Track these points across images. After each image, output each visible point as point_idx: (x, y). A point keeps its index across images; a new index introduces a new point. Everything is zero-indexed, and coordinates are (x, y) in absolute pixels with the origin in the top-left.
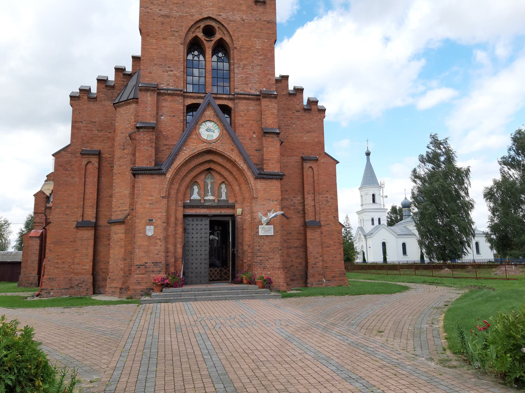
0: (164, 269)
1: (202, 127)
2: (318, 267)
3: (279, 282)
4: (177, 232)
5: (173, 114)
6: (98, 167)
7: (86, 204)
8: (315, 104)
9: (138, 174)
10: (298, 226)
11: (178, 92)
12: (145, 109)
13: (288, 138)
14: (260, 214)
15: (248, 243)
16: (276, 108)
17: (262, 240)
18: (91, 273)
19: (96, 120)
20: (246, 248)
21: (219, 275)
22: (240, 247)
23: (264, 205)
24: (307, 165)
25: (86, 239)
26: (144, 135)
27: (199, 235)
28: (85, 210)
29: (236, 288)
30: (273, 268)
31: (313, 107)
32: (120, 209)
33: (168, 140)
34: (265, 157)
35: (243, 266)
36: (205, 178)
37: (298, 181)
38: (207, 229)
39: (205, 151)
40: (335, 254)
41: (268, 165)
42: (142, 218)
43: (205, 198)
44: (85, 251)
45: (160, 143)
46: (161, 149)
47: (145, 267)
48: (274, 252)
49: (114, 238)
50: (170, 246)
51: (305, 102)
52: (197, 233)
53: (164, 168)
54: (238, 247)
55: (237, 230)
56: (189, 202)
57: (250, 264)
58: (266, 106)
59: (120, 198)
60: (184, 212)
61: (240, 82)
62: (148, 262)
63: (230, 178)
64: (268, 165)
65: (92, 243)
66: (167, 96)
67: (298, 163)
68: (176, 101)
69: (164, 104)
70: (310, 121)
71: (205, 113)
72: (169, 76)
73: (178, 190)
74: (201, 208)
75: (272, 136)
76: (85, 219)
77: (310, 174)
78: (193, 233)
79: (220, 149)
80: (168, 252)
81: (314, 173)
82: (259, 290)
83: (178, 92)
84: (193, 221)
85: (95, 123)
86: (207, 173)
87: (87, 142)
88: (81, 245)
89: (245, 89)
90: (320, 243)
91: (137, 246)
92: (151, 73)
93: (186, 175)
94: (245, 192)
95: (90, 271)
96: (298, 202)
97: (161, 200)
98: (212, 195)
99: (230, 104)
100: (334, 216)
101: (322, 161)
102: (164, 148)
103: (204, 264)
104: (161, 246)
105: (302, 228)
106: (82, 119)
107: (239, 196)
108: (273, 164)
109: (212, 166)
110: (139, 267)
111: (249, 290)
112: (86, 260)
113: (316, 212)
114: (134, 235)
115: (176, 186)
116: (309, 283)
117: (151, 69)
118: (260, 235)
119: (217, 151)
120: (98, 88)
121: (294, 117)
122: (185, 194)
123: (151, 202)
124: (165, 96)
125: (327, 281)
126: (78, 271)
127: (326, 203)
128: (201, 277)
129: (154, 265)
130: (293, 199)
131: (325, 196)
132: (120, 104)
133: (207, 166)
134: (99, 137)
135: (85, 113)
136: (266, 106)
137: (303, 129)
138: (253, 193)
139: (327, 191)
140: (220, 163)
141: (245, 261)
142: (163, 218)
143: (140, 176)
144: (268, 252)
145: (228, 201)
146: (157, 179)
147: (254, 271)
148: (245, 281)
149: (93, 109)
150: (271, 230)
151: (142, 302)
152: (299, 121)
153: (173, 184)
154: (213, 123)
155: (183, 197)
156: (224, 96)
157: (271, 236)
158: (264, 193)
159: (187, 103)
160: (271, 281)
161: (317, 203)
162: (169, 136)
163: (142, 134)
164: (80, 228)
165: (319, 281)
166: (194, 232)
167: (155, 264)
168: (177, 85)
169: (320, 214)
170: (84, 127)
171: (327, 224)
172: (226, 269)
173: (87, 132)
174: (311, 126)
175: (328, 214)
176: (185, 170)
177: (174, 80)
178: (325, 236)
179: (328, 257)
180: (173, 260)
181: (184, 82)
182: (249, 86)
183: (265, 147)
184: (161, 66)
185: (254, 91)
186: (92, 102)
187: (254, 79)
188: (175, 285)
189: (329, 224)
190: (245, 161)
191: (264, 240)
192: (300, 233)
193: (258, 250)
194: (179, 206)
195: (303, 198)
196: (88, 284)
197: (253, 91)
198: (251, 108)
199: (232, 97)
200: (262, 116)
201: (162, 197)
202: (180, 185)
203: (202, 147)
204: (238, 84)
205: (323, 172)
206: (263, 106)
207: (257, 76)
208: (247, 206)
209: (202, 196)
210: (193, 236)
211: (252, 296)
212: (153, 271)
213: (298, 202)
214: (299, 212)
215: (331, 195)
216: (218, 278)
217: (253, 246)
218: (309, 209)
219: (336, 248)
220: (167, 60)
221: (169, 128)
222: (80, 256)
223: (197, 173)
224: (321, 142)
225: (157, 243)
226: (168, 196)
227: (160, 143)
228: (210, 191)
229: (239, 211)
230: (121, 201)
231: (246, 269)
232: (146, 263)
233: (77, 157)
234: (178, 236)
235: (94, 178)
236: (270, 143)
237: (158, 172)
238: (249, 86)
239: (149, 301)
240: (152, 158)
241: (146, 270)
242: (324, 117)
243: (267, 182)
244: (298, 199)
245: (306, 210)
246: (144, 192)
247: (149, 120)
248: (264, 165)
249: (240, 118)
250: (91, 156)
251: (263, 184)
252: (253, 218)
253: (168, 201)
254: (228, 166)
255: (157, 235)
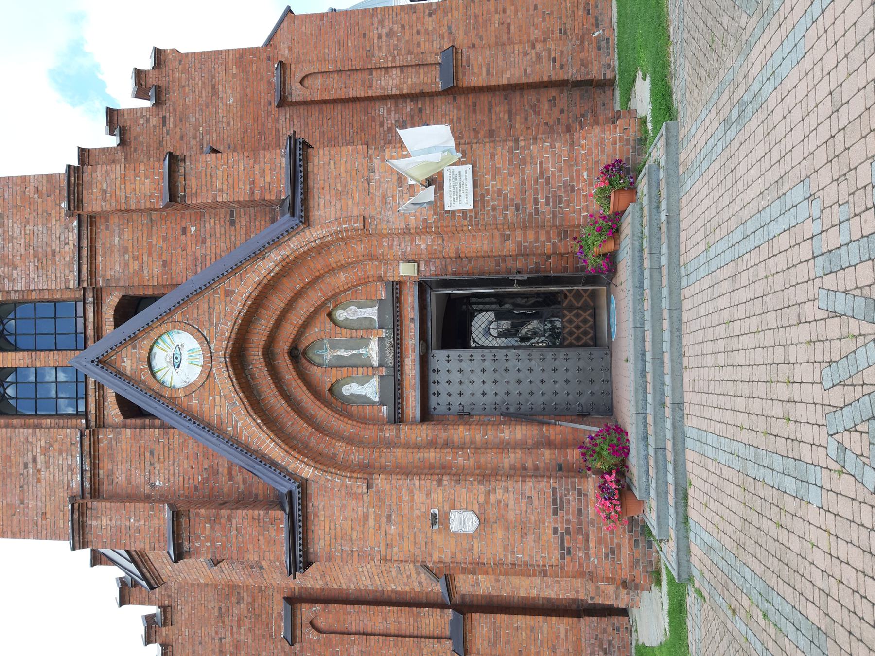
0: (573, 483)
1: (167, 380)
2: (562, 52)
3: (615, 143)
4: (467, 439)
5: (147, 454)
6: (322, 605)
7: (412, 631)
8: (143, 75)
9: (306, 553)
10: (455, 111)
11: (87, 442)
12: (132, 531)
13: (232, 145)
14: (406, 205)
15: (498, 241)
16: (109, 167)
17: (488, 201)
18: (575, 619)
19: (214, 606)
20: (511, 247)
21: (580, 311)
22: (509, 264)
23: (384, 197)
24: (297, 93)
25: (495, 631)
26: (198, 538)
27: (477, 377)
28: (425, 632)
29: (638, 272)
30: (572, 161)
31: (152, 81)
32: (414, 575)
33: (215, 467)
34: (244, 197)
35: (562, 255)
36: (320, 366)
37: (339, 115)
38: (460, 356)
39: (234, 369)
40: (528, 10)
41: (267, 187)
42: (427, 543)
43: (376, 364)
44: (524, 634)
45: (225, 490)
46: (241, 486)
47: (568, 533)
48: (524, 162)
49: (488, 588)
50: (506, 460)
51: (147, 104)
52: (472, 382)
53: (285, 487)
54: (509, 271)
55: (460, 274)
56: (385, 407)
57: (559, 234)
58: (103, 200)
59: (385, 574)
60: (412, 423)
61: (49, 273)
62: (553, 525)
63: (315, 297)
64: (267, 187)
65: (502, 619)
66: (101, 472)
67: (295, 117)
68: (111, 448)
69: (121, 479)
70: (187, 89)
71: (128, 373)
72: (47, 467)
73: (350, 441)
74: (402, 375)
75: (181, 178)
76: (447, 633)
77: (319, 80)
78: (472, 394)
79: (226, 329)
80: (524, 468)
81: (316, 71)
82: (645, 201)
83: (87, 442)
84: (439, 394)
85: (223, 610)
86: (304, 361)
87: (267, 625)
88: (508, 642)
89: (67, 259)
90: (500, 48)
91: (506, 558)
92: (44, 514)
93: (310, 420)
94: (351, 253)
95: (570, 622)
96: (393, 113)
97: (378, 491)
98: (367, 346)
99: (111, 301)
100: (427, 13)
101: (287, 52)
102: (239, 478)
103: (557, 363)
104: (506, 490)
105: (462, 100)
106: (213, 639)
107: (365, 272)
108: (263, 173)
109: (283, 346)
110: (566, 551)
111: (646, 231)
112: (545, 631)
113: (418, 62)
114: (478, 564)
115: (340, 448)
116: (605, 75)
117: (35, 512)
118: (472, 207)
119: (233, 336)
120: (142, 603)
121: (178, 129)
122: (364, 421)
123: (384, 519)
124: (101, 476)
125: (597, 27)
126: (571, 650)
127: (395, 39)
128: (592, 370)
129: (562, 509)
130: (385, 127)
131: (376, 41)
132: (148, 575)
133: (284, 364)
134: (254, 600)
135: (200, 631)
136: (103, 200)
137: (207, 107)
138: (351, 231)
139: (364, 35)
140: (270, 325)
141: (548, 248)
142: (428, 485)
143: (311, 550)
144: (523, 181)
145: (380, 301)
146: (318, 503)
147: (579, 220)
148: (610, 247)
149: (190, 615)
150: (456, 172)
151: (685, 576)
152: (188, 118)
153: (334, 456)
154: (156, 350)
155: (371, 427)
156: (90, 316)
157: (474, 173)
158: (349, 196)
159: (116, 416)
160: (613, 165)
161: (394, 60)
162: (206, 466)
163: (198, 544)
164: (469, 645)
165: (599, 48)
166: (467, 389)
167: (557, 505)
168: (69, 444)
169: (422, 53)
170: (232, 633)
171: (450, 33)
172: (566, 297)
173: (243, 628)
174: (200, 84)
175: (423, 31)
176: (293, 424)
177: (57, 454)
178: (481, 39)
179: (536, 29)
180: (547, 453)
181: (63, 427)
182: (58, 249)
183: (215, 197)
184: (26, 487)
185: (71, 234)
186: (175, 617)
187: (40, 236)
188: (621, 450)
189: (450, 28)
190: (258, 254)
191: (488, 194)
192: (475, 105)
193: (518, 209)
194: (397, 436)
195: (384, 98)
196: (604, 626)
197: (71, 238)
198: (117, 240)
199: (91, 295)
200: (133, 207)
201: (368, 488)
202: (336, 436)
203: (224, 380)
204: (54, 279)
205: (315, 47)
206: (106, 207)
207: (30, 227)
208: (391, 247)
209: (370, 373)
210: (478, 394)
211: (668, 223)
212: (580, 511)
213: (393, 113)
214: (420, 110)
215: (373, 24)
216: (590, 315)
217: (506, 227)
218: (410, 82)
219: (513, 8)
220: (9, 471)
221: (186, 466)
222: (536, 645)
223: (304, 388)
224: (237, 56)
225: (499, 502)
226: (367, 471)
227: (225, 490)
228: (355, 352)
229: (406, 270)
230: (394, 574)
231: (572, 246)
232: (555, 531)
233: (302, 648)
234: (478, 438)
235: (350, 613)
236: (204, 182)
237: (296, 501)
238: (58, 249)
239: (681, 553)
240: (261, 517)
241: (574, 532)
242: (175, 51)
243: (316, 190)
244: (385, 112)
245: (413, 91)
246: (354, 538)
247: (162, 522)
248: (267, 198)
249: (145, 271)
250: (298, 622)
251: (322, 202)
252: (425, 230)
253: (383, 470)
254: (277, 303)
255: (475, 502)
